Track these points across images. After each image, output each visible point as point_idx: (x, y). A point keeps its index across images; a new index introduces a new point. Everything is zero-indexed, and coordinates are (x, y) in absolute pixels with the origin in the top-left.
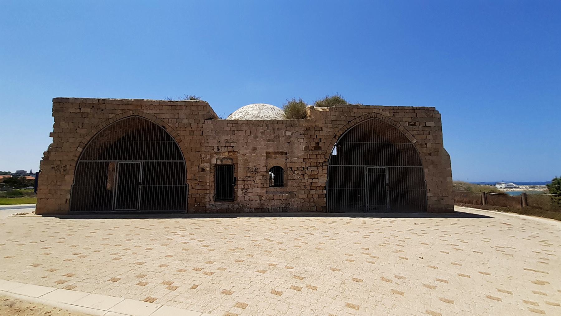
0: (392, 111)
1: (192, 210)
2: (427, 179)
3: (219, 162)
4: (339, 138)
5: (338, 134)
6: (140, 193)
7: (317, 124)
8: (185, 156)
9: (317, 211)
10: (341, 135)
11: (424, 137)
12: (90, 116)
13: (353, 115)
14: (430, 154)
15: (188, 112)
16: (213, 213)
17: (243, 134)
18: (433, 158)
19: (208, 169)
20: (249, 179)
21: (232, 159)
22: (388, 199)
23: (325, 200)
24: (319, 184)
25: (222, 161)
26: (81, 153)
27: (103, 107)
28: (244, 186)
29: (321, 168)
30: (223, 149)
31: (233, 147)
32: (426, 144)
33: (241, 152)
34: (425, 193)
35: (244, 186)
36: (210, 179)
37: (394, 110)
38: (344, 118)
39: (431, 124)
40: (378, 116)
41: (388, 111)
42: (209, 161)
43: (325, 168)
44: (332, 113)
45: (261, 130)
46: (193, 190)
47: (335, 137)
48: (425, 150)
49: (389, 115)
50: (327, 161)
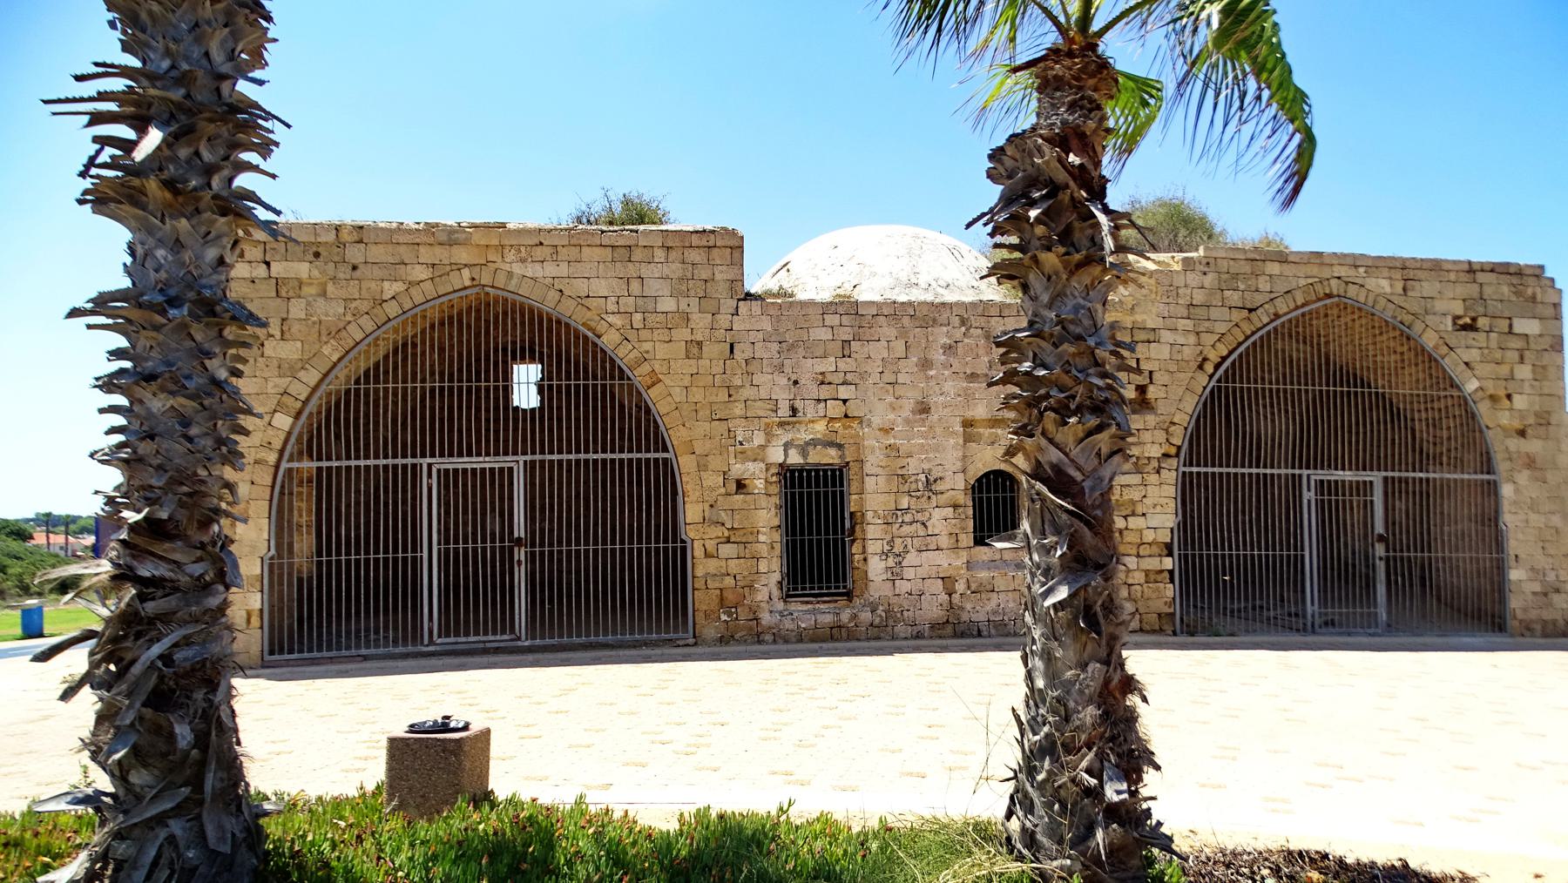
0: (1399, 276)
1: (710, 631)
2: (1509, 519)
3: (795, 458)
4: (1217, 367)
5: (1214, 357)
6: (520, 575)
7: (1139, 318)
8: (676, 435)
9: (1141, 630)
10: (1224, 359)
11: (1504, 370)
12: (306, 290)
13: (1264, 285)
14: (1522, 433)
15: (675, 269)
16: (786, 641)
17: (878, 351)
18: (1533, 446)
19: (760, 484)
20: (908, 518)
21: (840, 446)
22: (1381, 589)
23: (1169, 591)
24: (1149, 536)
25: (804, 454)
26: (289, 434)
27: (355, 254)
28: (891, 542)
29: (1153, 478)
30: (809, 410)
31: (845, 401)
32: (1509, 397)
33: (877, 421)
34: (1500, 568)
35: (891, 542)
36: (766, 517)
37: (1407, 271)
38: (1234, 298)
39: (1525, 326)
40: (1352, 291)
41: (1386, 273)
42: (758, 455)
43: (1170, 476)
44: (1193, 279)
45: (941, 336)
46: (711, 565)
47: (1201, 367)
48: (1505, 419)
49: (1388, 290)
50: (1173, 451)
